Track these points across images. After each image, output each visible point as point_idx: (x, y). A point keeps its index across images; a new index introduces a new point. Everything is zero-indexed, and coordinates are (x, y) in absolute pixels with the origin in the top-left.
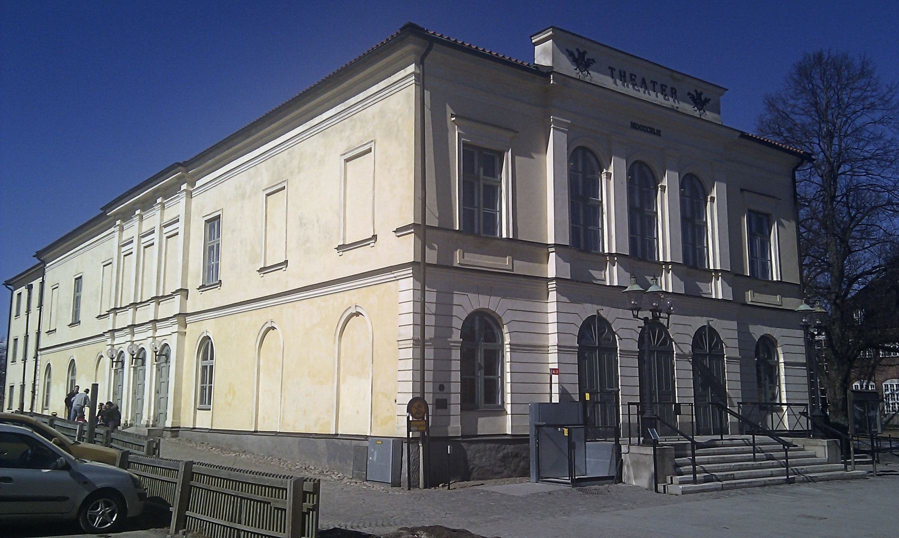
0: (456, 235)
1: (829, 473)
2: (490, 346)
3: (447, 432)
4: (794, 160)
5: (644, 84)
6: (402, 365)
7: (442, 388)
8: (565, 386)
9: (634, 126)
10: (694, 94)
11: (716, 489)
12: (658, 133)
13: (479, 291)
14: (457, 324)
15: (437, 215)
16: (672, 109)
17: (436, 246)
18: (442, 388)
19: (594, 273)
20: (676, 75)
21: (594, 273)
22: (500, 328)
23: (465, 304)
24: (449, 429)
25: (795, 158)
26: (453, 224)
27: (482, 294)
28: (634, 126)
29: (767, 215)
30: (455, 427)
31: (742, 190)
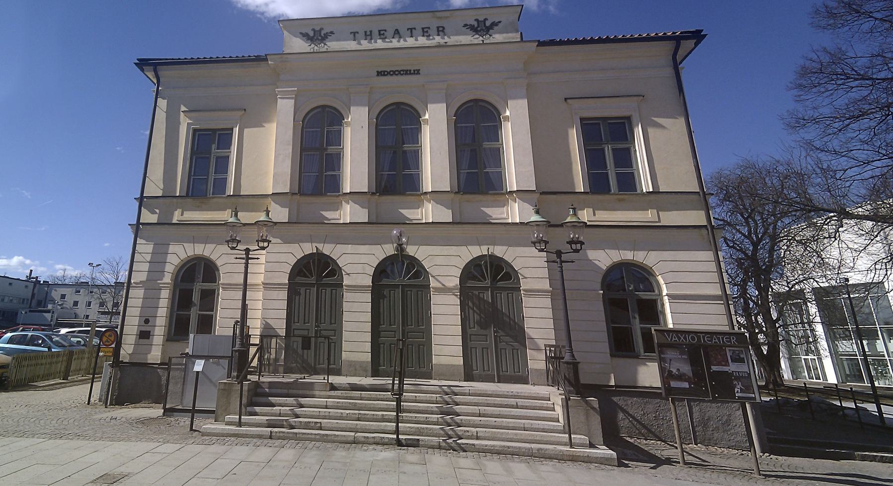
0: (179, 200)
1: (527, 445)
2: (208, 286)
3: (147, 359)
4: (669, 46)
5: (397, 33)
6: (277, 305)
7: (147, 321)
8: (268, 321)
9: (379, 74)
10: (476, 24)
11: (260, 437)
12: (417, 72)
13: (194, 240)
14: (170, 268)
15: (162, 186)
16: (439, 46)
17: (157, 211)
18: (147, 321)
19: (328, 214)
20: (439, 14)
21: (328, 214)
22: (653, 275)
23: (179, 253)
24: (149, 356)
25: (160, 73)
26: (573, 184)
27: (198, 243)
28: (379, 74)
29: (629, 118)
30: (155, 355)
31: (566, 99)
